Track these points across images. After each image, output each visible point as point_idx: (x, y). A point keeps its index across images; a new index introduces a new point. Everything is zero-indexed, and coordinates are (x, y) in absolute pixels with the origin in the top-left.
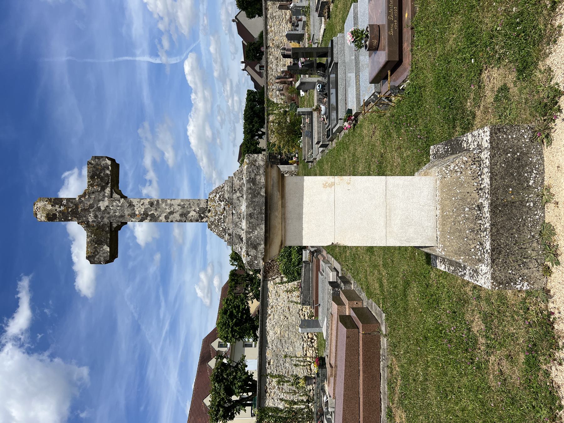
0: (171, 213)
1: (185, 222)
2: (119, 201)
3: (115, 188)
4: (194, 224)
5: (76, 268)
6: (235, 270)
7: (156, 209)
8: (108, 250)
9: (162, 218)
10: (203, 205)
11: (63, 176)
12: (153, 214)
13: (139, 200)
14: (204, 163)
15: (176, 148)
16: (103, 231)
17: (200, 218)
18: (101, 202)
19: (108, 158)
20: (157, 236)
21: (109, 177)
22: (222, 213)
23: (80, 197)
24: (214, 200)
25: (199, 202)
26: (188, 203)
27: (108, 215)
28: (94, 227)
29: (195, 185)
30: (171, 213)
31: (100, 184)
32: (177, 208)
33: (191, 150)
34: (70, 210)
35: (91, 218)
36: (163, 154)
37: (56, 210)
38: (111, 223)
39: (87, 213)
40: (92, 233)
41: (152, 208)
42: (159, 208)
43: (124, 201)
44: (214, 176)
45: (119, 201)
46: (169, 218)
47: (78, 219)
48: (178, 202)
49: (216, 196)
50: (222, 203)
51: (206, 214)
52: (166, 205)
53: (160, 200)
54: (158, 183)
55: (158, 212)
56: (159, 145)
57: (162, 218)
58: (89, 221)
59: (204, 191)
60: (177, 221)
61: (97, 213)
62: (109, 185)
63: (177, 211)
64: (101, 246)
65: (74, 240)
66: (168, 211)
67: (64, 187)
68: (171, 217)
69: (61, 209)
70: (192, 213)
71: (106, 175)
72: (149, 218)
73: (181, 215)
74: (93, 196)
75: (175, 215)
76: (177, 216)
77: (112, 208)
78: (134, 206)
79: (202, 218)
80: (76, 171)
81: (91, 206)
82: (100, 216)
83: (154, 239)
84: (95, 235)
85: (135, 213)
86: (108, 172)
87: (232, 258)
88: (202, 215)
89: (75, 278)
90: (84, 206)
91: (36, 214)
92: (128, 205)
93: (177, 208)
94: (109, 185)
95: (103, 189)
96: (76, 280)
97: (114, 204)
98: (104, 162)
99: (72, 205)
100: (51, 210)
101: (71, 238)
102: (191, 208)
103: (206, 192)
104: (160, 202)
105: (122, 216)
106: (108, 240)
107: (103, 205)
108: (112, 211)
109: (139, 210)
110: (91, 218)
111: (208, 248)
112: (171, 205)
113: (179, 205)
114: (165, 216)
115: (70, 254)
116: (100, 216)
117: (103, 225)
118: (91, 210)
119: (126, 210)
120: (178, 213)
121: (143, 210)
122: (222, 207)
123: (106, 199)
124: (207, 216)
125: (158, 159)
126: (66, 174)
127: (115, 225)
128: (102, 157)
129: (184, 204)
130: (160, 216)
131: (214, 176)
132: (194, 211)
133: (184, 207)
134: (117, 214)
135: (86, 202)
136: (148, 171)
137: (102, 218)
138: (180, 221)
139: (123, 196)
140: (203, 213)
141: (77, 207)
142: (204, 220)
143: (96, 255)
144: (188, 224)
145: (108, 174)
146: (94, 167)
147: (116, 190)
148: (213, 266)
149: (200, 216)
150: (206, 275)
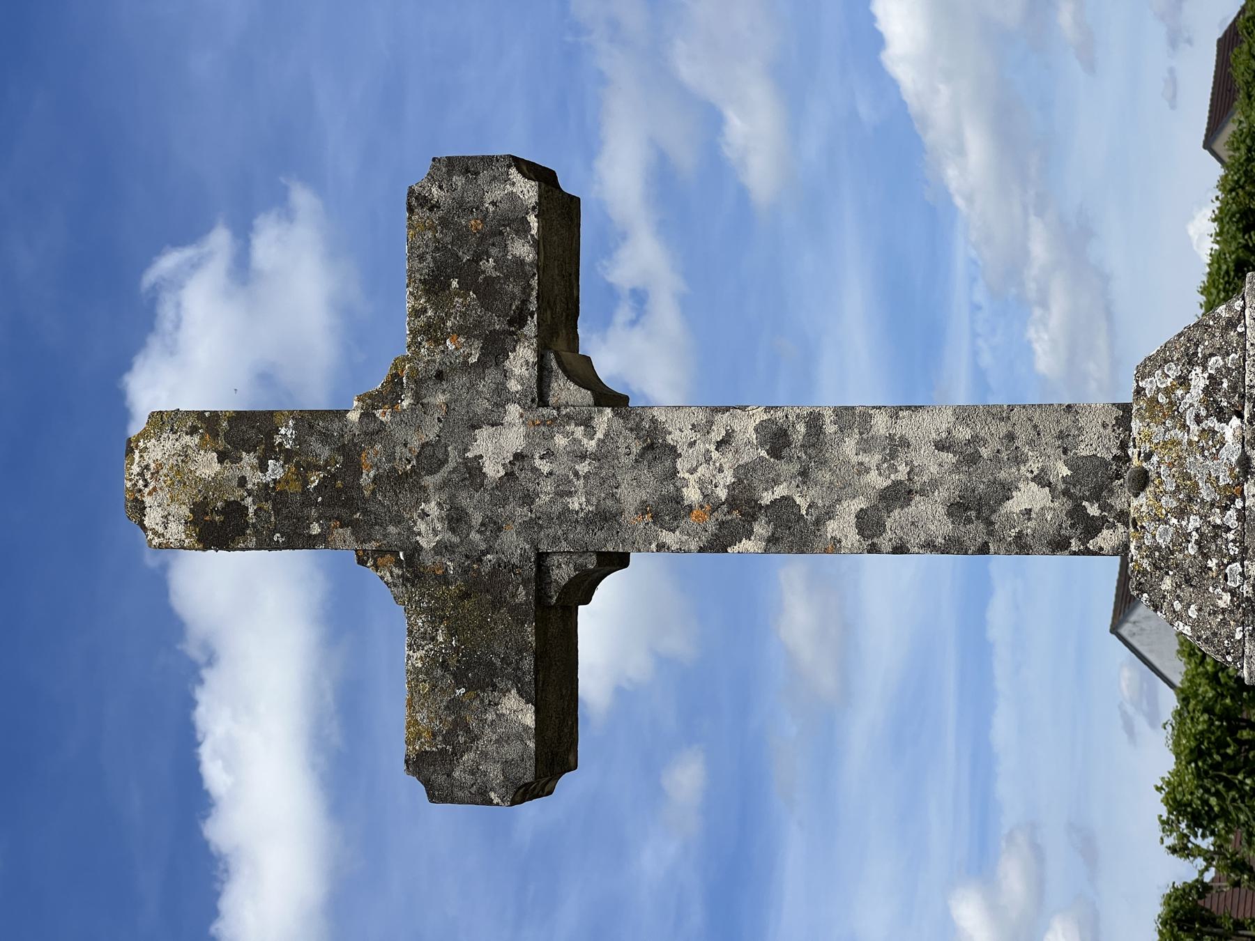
0: (898, 495)
1: (983, 550)
2: (587, 423)
3: (561, 344)
4: (1044, 565)
5: (223, 830)
6: (1201, 888)
7: (804, 473)
8: (529, 719)
9: (842, 526)
10: (1095, 443)
11: (150, 277)
12: (787, 501)
13: (701, 417)
14: (967, 165)
15: (793, 82)
16: (496, 604)
17: (1075, 533)
18: (483, 433)
19: (518, 163)
20: (678, 644)
21: (527, 278)
22: (1232, 494)
23: (372, 402)
24: (1174, 412)
25: (1067, 422)
26: (1003, 429)
27: (522, 513)
28: (444, 580)
29: (912, 319)
30: (898, 495)
31: (478, 324)
32: (932, 464)
33: (884, 84)
34: (315, 480)
35: (429, 531)
36: (713, 120)
37: (242, 481)
38: (541, 557)
39: (406, 498)
40: (435, 616)
41: (784, 468)
42: (823, 463)
43: (618, 424)
44: (1040, 249)
45: (587, 423)
46: (880, 527)
47: (360, 531)
48: (938, 424)
49: (1184, 381)
50: (1231, 430)
51: (1118, 503)
52: (865, 446)
53: (829, 417)
54: (685, 305)
55: (813, 492)
56: (689, 67)
57: (842, 526)
58: (418, 548)
59: (975, 353)
60: (929, 546)
61: (464, 499)
62: (531, 328)
63: (935, 484)
64: (488, 696)
65: (211, 660)
66: (878, 481)
67: (154, 342)
68: (895, 519)
69: (268, 477)
70: (1028, 497)
71: (503, 267)
72: (761, 529)
73: (957, 509)
74: (441, 398)
75: (919, 506)
76: (930, 514)
77: (545, 467)
78: (673, 452)
79: (1092, 528)
80: (220, 239)
81: (430, 458)
82: (477, 518)
83: (663, 662)
84: (451, 633)
85: (678, 499)
86: (522, 250)
87: (1177, 805)
88: (1093, 510)
89: (218, 895)
90: (391, 457)
91: (140, 508)
92: (636, 448)
93: (932, 464)
94: (531, 328)
95: (496, 350)
96: (225, 904)
97: (560, 441)
98: (497, 193)
99: (325, 453)
100: (217, 483)
101: (193, 651)
102: (1019, 460)
103: (986, 359)
104: (830, 428)
105: (605, 518)
106: (528, 663)
107: (493, 450)
108: (548, 487)
109: (703, 477)
110: (429, 531)
111: (1003, 728)
112: (896, 446)
113: (941, 446)
114: (861, 515)
115: (185, 742)
116: (477, 518)
117: (495, 571)
118: (429, 481)
119: (626, 478)
120: (941, 495)
121: (728, 477)
122: (1231, 451)
123: (514, 410)
124: (1123, 516)
125: (686, 159)
126: (169, 262)
127: (562, 572)
128: (489, 161)
129: (975, 440)
130: (829, 514)
131: (1040, 249)
132: (1041, 479)
133: (974, 459)
134: (575, 503)
135: (400, 434)
136: (624, 236)
137: (493, 527)
138: (953, 546)
139: (607, 398)
140: (1096, 496)
141: (353, 465)
142: (1107, 538)
143: (458, 752)
144: (1000, 564)
145: (520, 262)
146: (444, 222)
147: (566, 355)
148: (1038, 852)
149: (1077, 513)
150: (994, 909)
